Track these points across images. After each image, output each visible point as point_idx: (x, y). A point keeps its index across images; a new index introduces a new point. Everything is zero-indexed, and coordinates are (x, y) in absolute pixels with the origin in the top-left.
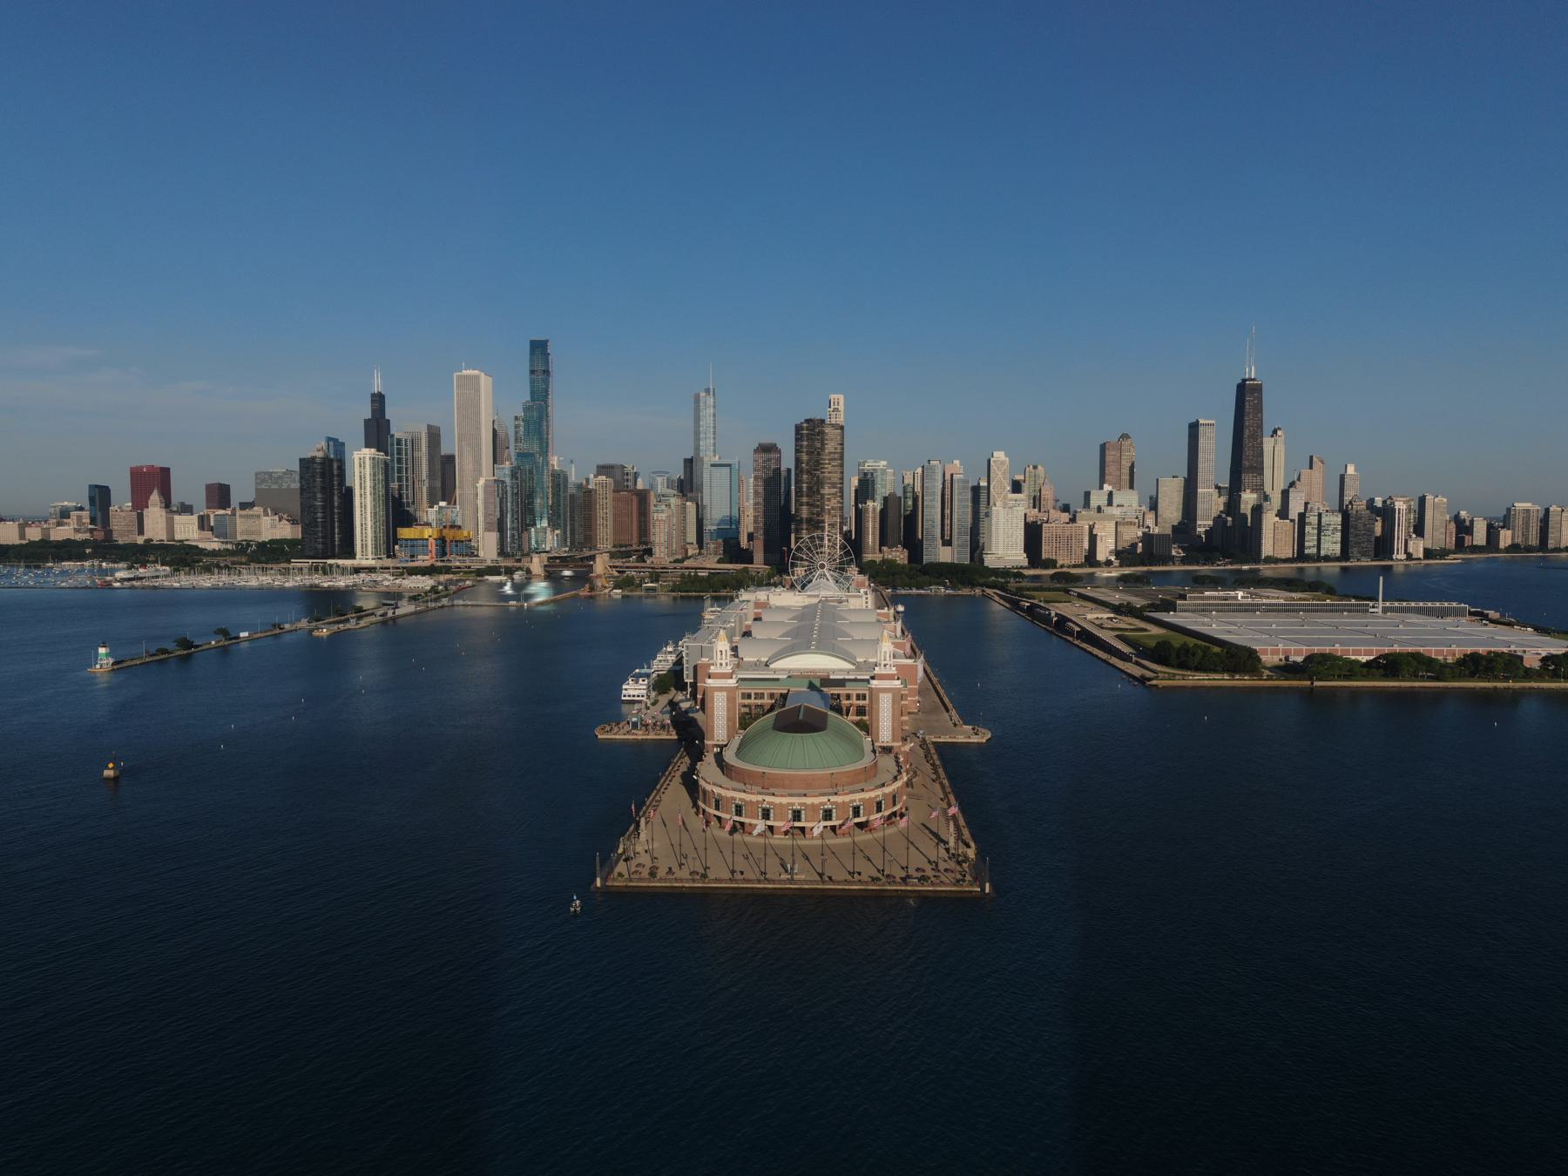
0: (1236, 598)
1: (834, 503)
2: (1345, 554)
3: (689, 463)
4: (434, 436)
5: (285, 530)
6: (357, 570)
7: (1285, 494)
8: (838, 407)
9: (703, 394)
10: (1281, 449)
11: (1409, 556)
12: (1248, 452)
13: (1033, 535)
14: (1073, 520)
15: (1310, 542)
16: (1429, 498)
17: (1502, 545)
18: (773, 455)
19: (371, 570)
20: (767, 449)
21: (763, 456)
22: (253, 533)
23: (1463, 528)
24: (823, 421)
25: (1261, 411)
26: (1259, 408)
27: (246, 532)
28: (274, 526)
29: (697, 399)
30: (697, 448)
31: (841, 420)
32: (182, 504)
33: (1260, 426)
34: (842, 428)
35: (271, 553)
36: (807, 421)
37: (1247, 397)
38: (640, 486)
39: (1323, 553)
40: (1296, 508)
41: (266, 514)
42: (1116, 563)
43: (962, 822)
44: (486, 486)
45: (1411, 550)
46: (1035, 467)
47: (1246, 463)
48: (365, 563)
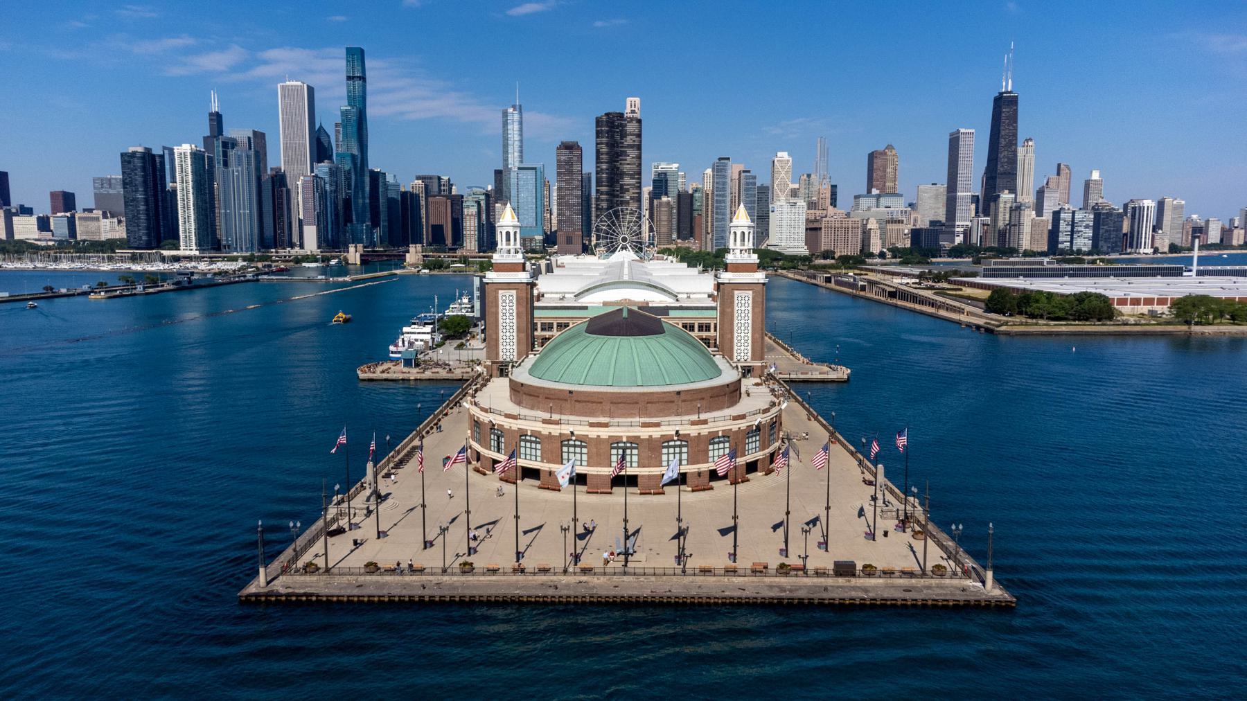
0: (1042, 263)
1: (633, 206)
2: (1095, 249)
3: (498, 173)
4: (259, 140)
5: (120, 233)
6: (176, 259)
7: (1040, 194)
8: (632, 105)
9: (511, 110)
10: (1031, 155)
11: (1156, 251)
12: (1003, 155)
13: (813, 230)
14: (577, 557)
15: (1064, 238)
16: (1168, 200)
17: (1235, 243)
18: (576, 153)
19: (189, 258)
20: (569, 147)
21: (565, 154)
22: (93, 234)
23: (1199, 231)
24: (621, 115)
25: (1016, 122)
26: (1014, 118)
27: (87, 233)
28: (112, 230)
29: (505, 114)
30: (506, 160)
31: (638, 115)
32: (22, 207)
33: (1015, 135)
34: (639, 121)
35: (107, 247)
36: (607, 114)
37: (1004, 108)
38: (454, 192)
39: (1075, 248)
40: (1049, 207)
41: (105, 216)
42: (889, 255)
43: (890, 484)
44: (304, 183)
45: (1157, 244)
46: (809, 176)
47: (1000, 169)
48: (188, 253)
